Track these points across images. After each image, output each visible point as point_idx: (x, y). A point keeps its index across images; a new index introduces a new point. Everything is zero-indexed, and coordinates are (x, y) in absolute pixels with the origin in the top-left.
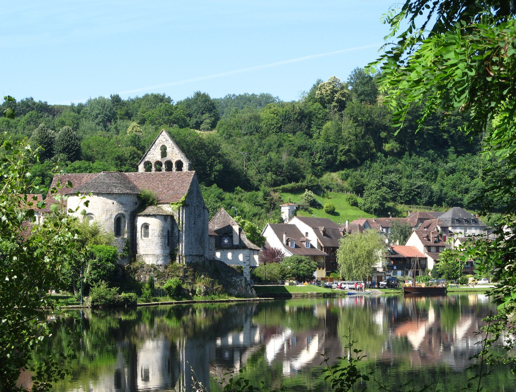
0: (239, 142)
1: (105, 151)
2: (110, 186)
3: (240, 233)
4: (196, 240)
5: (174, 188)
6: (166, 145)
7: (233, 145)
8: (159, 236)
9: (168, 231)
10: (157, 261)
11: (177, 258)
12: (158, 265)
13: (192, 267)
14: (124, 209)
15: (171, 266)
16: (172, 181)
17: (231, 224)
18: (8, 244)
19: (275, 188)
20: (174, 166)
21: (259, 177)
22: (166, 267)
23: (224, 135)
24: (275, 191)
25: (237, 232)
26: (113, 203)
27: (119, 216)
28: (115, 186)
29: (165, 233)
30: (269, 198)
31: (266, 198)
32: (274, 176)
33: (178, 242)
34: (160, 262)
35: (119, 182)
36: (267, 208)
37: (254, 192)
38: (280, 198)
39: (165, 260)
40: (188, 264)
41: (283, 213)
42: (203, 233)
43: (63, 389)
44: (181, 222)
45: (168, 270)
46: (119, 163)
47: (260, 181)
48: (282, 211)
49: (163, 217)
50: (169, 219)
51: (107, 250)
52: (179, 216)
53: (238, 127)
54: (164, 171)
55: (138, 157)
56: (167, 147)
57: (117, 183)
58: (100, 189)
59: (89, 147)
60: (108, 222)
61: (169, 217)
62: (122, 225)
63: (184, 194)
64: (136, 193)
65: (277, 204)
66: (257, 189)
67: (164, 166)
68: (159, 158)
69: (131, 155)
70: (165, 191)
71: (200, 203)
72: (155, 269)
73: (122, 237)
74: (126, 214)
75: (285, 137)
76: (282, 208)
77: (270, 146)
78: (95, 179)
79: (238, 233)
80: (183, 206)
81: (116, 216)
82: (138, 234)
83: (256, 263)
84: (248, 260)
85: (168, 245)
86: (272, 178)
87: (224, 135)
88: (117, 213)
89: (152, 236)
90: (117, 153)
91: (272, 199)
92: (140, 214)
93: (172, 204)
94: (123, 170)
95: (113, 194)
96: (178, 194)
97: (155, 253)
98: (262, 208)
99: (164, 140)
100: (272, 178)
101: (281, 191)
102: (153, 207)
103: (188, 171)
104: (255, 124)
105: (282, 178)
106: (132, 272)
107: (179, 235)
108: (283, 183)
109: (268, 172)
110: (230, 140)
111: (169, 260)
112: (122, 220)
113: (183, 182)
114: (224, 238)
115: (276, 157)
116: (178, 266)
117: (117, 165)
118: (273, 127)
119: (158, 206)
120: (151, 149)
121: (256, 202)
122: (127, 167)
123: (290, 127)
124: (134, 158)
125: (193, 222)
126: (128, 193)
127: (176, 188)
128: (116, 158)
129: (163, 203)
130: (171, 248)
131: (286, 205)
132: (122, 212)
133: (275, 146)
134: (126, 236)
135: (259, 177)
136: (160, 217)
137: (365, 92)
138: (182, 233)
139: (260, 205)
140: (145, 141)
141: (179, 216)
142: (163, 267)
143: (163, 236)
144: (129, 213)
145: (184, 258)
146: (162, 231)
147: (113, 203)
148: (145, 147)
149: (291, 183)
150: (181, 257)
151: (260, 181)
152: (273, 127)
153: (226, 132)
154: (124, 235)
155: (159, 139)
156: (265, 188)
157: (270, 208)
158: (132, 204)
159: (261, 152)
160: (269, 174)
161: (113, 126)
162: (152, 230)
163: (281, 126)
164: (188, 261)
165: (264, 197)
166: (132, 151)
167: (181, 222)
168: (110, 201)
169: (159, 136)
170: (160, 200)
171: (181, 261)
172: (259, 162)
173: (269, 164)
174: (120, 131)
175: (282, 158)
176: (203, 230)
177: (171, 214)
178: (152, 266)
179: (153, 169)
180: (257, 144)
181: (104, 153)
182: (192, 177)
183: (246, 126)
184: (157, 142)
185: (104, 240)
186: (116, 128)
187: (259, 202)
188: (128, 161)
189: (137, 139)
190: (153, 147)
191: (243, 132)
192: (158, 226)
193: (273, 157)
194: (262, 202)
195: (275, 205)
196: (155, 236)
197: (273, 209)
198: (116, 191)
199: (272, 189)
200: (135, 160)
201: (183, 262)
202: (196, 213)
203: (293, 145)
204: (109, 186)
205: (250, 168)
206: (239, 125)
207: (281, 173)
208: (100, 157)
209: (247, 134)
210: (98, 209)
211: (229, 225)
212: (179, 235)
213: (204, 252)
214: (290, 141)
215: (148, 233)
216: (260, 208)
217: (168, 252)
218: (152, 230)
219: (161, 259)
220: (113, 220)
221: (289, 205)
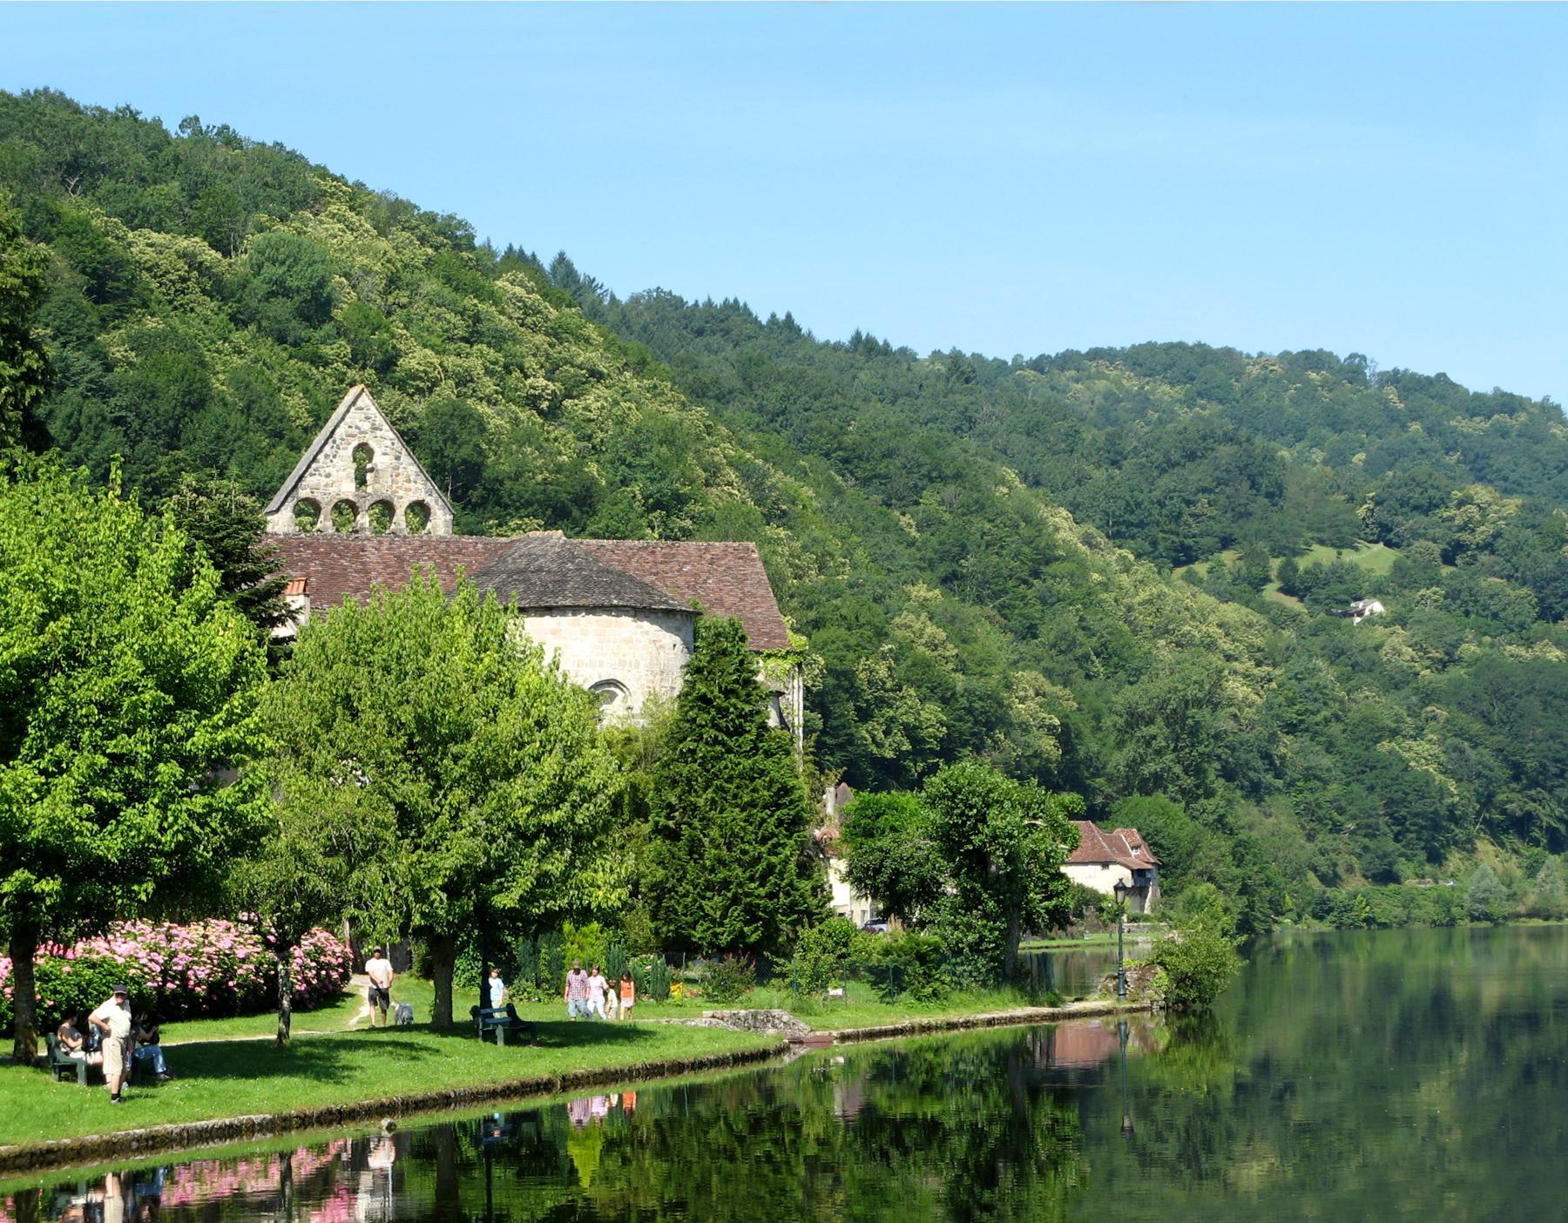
6: (372, 444)
18: (1464, 1216)
43: (1567, 906)
68: (348, 489)
99: (366, 426)
120: (321, 457)
137: (1304, 510)
210: (637, 665)
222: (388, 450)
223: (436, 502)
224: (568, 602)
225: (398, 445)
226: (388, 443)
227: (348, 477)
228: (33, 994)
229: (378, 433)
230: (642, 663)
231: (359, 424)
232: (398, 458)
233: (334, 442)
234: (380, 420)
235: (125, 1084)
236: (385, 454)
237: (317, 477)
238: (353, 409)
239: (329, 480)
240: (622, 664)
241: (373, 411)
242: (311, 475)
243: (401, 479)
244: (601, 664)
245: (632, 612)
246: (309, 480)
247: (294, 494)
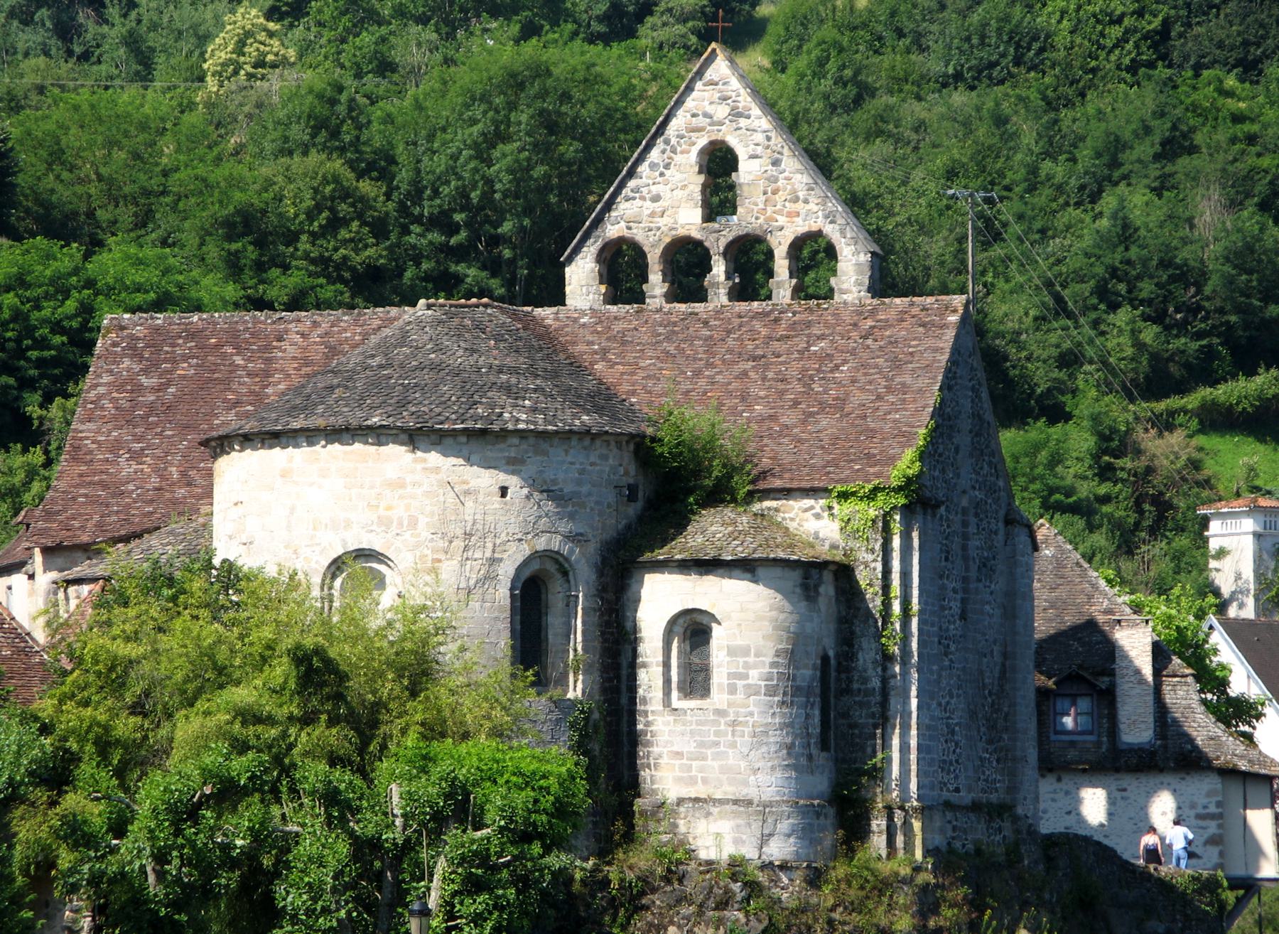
0: (920, 127)
1: (154, 184)
2: (482, 390)
3: (1157, 672)
4: (973, 714)
5: (841, 402)
6: (732, 141)
7: (882, 148)
8: (771, 691)
9: (825, 659)
10: (764, 840)
11: (878, 823)
12: (767, 866)
13: (963, 881)
14: (565, 526)
15: (841, 871)
16: (825, 357)
17: (1101, 618)
19: (1161, 406)
20: (781, 266)
21: (1058, 336)
22: (815, 878)
23: (826, 84)
24: (1165, 424)
25: (1145, 666)
26: (504, 491)
27: (535, 566)
28: (507, 389)
29: (808, 673)
30: (1127, 462)
31: (1110, 468)
32: (1149, 334)
33: (884, 721)
34: (778, 850)
35: (522, 361)
36: (1117, 525)
37: (1037, 430)
38: (1195, 465)
39: (806, 833)
40: (943, 857)
41: (1221, 553)
42: (1003, 672)
44: (896, 607)
45: (826, 896)
46: (252, 253)
47: (1070, 360)
48: (1214, 545)
49: (796, 575)
50: (827, 589)
51: (520, 774)
52: (887, 572)
53: (900, 34)
54: (720, 297)
55: (360, 216)
56: (741, 153)
57: (514, 371)
58: (423, 408)
59: (57, 156)
60: (475, 605)
61: (828, 576)
62: (554, 622)
63: (908, 438)
64: (631, 429)
65: (1182, 504)
66: (1057, 415)
67: (719, 269)
69: (319, 208)
70: (790, 417)
71: (992, 490)
72: (753, 888)
73: (555, 692)
74: (574, 553)
75: (1204, 96)
76: (1215, 526)
77: (1113, 151)
78: (385, 347)
79: (1147, 671)
80: (907, 510)
81: (519, 570)
82: (642, 676)
83: (1258, 852)
84: (1214, 841)
85: (824, 745)
86: (1139, 346)
87: (826, 84)
88: (526, 550)
89: (732, 690)
90: (238, 196)
91: (1150, 470)
92: (661, 554)
93: (844, 496)
94: (272, 293)
95: (504, 434)
96: (871, 434)
97: (751, 792)
98: (1091, 528)
99: (722, 112)
100: (1139, 346)
101: (1194, 423)
102: (728, 512)
103: (869, 301)
104: (1006, 19)
105: (1195, 345)
106: (613, 904)
107: (885, 681)
108: (1204, 372)
109: (1114, 307)
110: (862, 118)
111: (830, 837)
112: (555, 594)
113: (897, 364)
114: (1061, 704)
115: (1159, 214)
116: (886, 868)
117: (234, 267)
118: (1115, 32)
119: (756, 507)
120: (643, 168)
121: (1052, 490)
122: (295, 279)
123: (1221, 34)
124: (336, 223)
125: (956, 606)
126: (586, 433)
127: (857, 398)
128: (228, 224)
129: (787, 493)
130: (837, 761)
131: (1239, 505)
132: (556, 543)
133: (1145, 149)
134: (575, 690)
135: (1058, 336)
136: (777, 572)
138: (905, 673)
139: (1075, 509)
140: (389, 119)
141: (887, 572)
142: (798, 877)
143: (797, 691)
144: (592, 547)
145: (917, 825)
146: (793, 655)
147: (504, 491)
148: (392, 161)
149: (1251, 373)
150: (898, 817)
151: (1070, 360)
152: (1115, 32)
153: (832, 66)
154: (562, 681)
155: (690, 103)
156: (1098, 408)
157: (1137, 525)
158: (611, 497)
159: (1060, 188)
160: (1123, 317)
161: (115, 31)
162: (732, 652)
163: (1166, 24)
164: (938, 840)
165: (1096, 457)
166: (325, 181)
167: (896, 607)
168: (485, 479)
169: (689, 89)
170: (763, 475)
171: (900, 840)
172: (1054, 245)
173: (1116, 257)
174: (160, 59)
175: (1190, 222)
176: (1005, 655)
177: (838, 556)
178: (736, 867)
179: (656, 284)
180: (1028, 133)
181: (147, 193)
182: (950, 334)
183: (952, 29)
184: (677, 124)
185: (470, 710)
186: (132, 42)
187: (1069, 492)
188: (304, 244)
189: (341, 109)
190: (654, 155)
191: (935, 65)
192: (767, 627)
193: (1137, 217)
194: (1085, 489)
195: (1163, 506)
196: (751, 691)
197: (1154, 531)
198: (518, 417)
199: (1144, 407)
200: (344, 234)
201: (909, 847)
202: (973, 553)
203: (1251, 139)
204: (471, 388)
205: (1001, 284)
206: (909, 26)
207: (1194, 310)
208: (126, 215)
209: (958, 76)
210: (413, 523)
211: (1091, 625)
212: (885, 681)
213: (1013, 789)
214: (1238, 118)
215: (705, 670)
216: (1080, 523)
217: (821, 783)
218: (732, 652)
219: (784, 826)
220: (502, 593)
221: (1254, 510)
222: (759, 150)
224: (321, 422)
225: (778, 141)
226: (760, 137)
227: (690, 198)
228: (331, 928)
229: (743, 122)
230: (423, 521)
232: (776, 163)
233: (667, 142)
234: (745, 99)
237: (638, 202)
238: (699, 85)
239: (658, 207)
240: (385, 523)
241: (735, 83)
242: (627, 199)
243: (780, 198)
244: (348, 524)
245: (404, 437)
247: (598, 232)
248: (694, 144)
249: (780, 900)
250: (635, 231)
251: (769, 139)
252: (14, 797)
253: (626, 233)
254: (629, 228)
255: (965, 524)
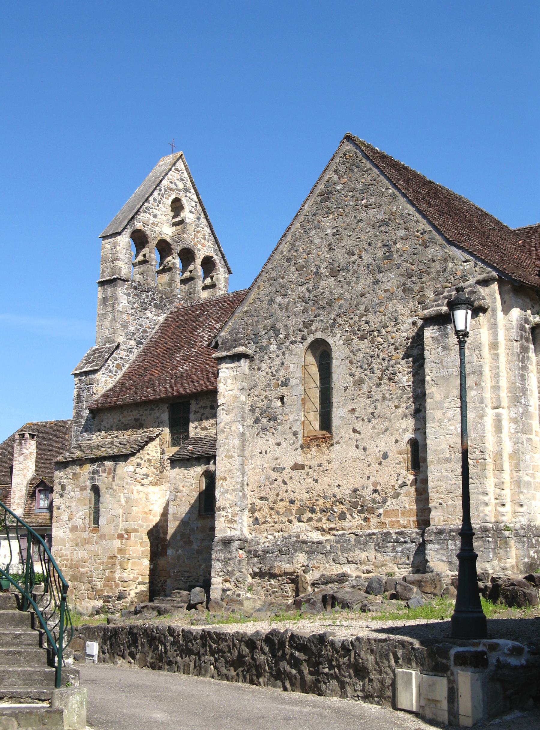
99: (181, 186)
223: (220, 260)
231: (177, 182)
232: (198, 218)
233: (160, 190)
235: (395, 593)
236: (191, 212)
246: (143, 216)
248: (170, 196)
249: (147, 641)
250: (146, 229)
251: (196, 205)
252: (10, 444)
253: (142, 228)
254: (144, 226)
255: (203, 705)
